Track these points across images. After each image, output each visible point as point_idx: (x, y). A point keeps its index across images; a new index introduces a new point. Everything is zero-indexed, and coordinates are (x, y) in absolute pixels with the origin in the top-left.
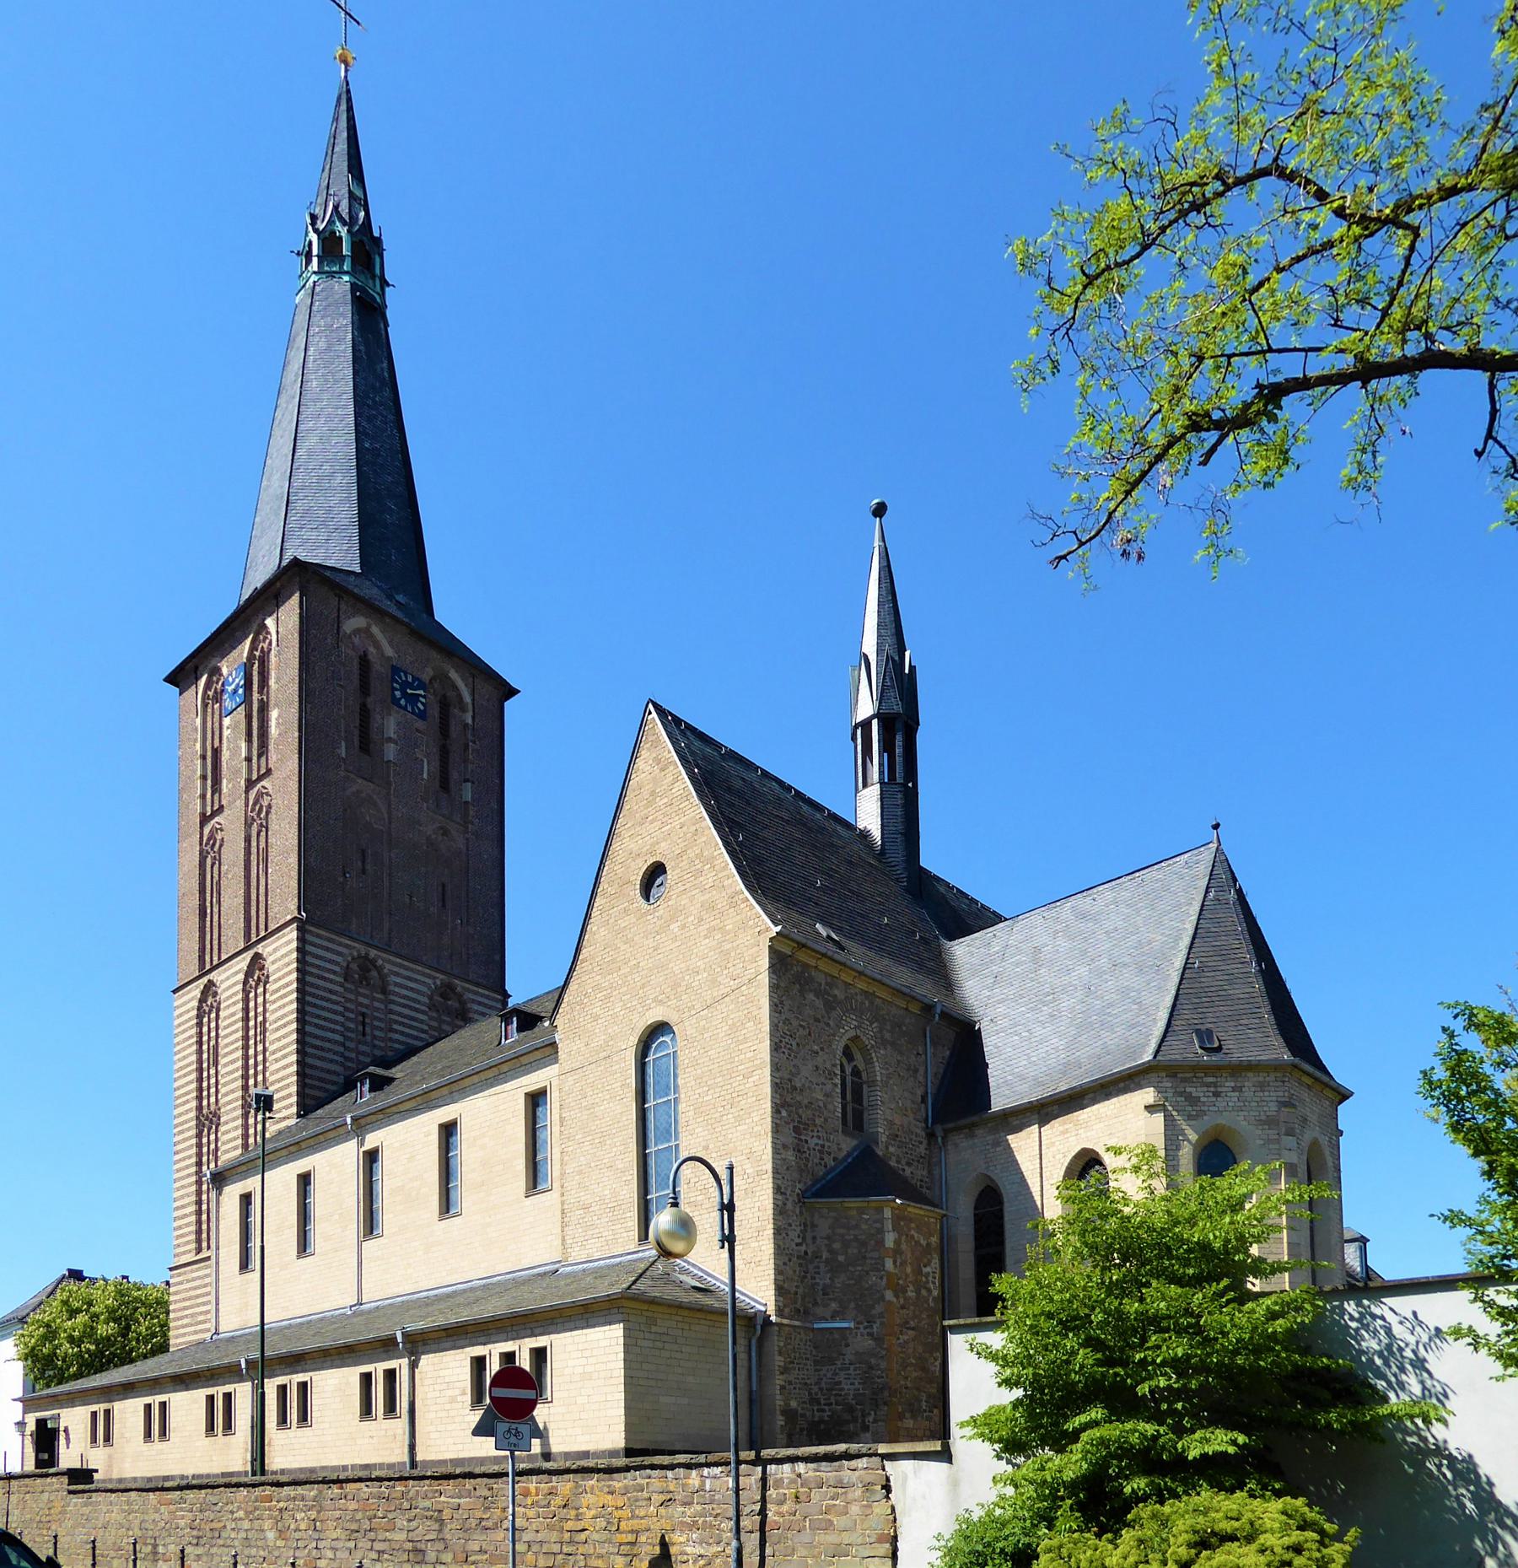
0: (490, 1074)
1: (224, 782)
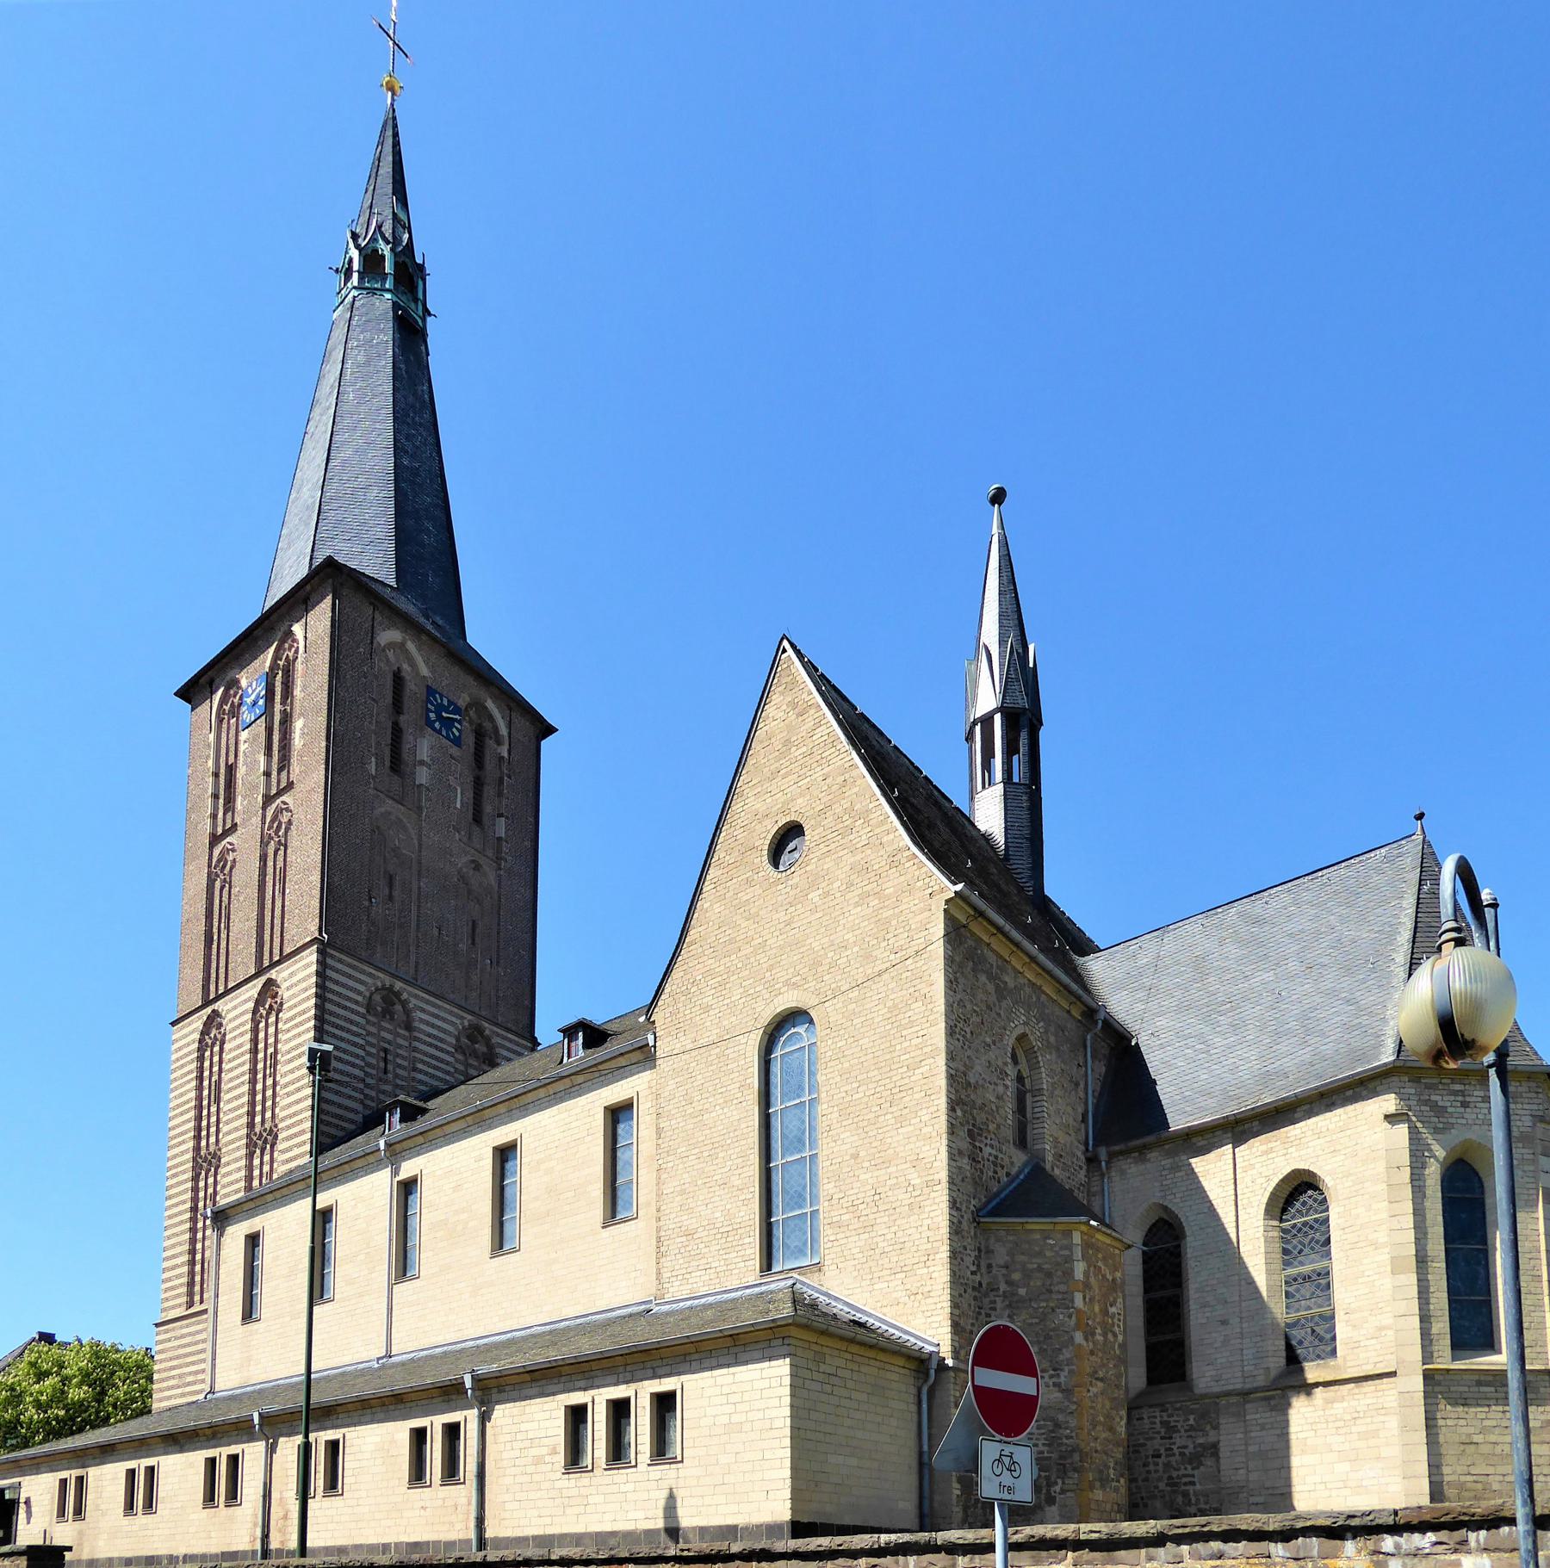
0: (560, 1086)
1: (239, 800)
